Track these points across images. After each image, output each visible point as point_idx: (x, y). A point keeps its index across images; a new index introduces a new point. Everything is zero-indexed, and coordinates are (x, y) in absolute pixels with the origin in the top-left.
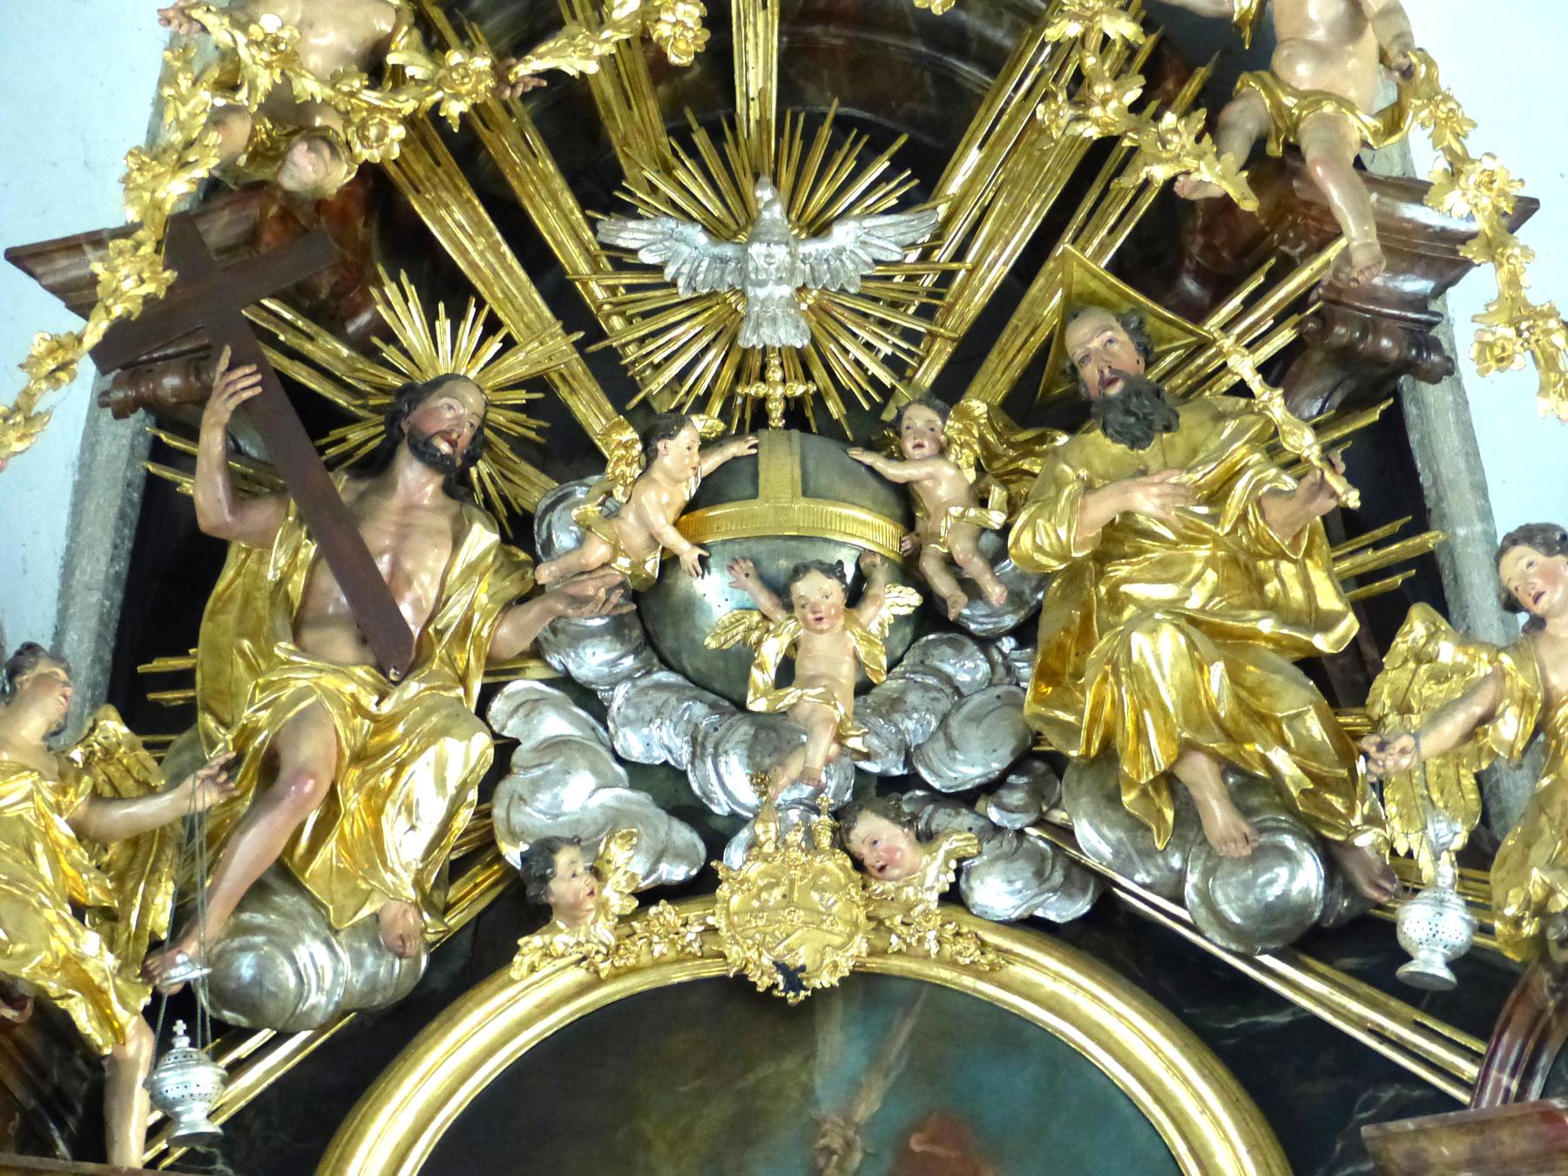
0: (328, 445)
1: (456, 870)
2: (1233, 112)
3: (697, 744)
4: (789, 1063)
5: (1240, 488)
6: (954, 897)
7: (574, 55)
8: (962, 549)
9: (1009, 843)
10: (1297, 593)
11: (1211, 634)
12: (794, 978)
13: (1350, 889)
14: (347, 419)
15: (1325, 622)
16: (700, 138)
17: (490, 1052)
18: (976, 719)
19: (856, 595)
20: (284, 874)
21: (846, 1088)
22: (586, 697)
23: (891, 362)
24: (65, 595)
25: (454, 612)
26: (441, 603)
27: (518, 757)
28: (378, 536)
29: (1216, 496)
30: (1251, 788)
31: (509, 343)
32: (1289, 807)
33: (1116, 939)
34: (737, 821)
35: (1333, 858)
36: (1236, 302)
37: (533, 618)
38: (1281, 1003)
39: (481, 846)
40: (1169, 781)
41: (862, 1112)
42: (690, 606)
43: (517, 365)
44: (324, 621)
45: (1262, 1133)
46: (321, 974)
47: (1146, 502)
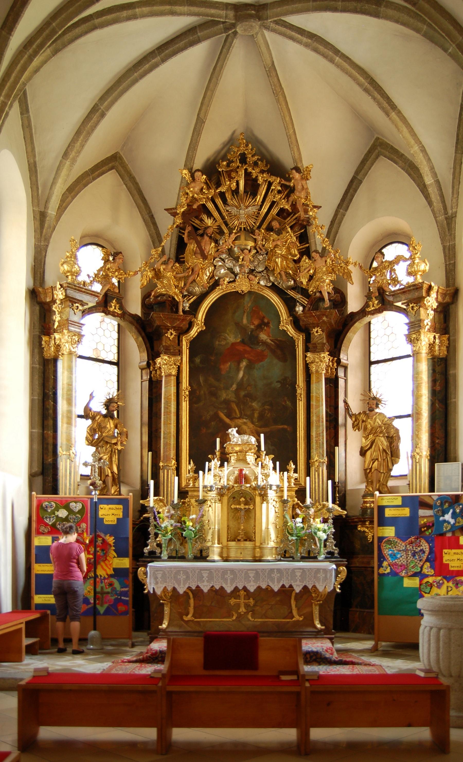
0: (198, 233)
1: (211, 279)
2: (290, 198)
3: (234, 266)
4: (242, 300)
5: (288, 241)
6: (259, 283)
7: (222, 189)
8: (261, 246)
9: (264, 277)
10: (294, 252)
11: (284, 257)
12: (243, 291)
13: (296, 284)
14: (200, 230)
15: (296, 256)
16: (235, 196)
17: (214, 298)
18: (261, 264)
19: (250, 251)
20: (194, 281)
21: (247, 303)
22: (223, 260)
23: (254, 223)
24: (171, 244)
25: (210, 253)
26: (209, 251)
27: (216, 267)
28: (203, 244)
29: (286, 242)
30: (287, 274)
31: (216, 221)
32: (291, 276)
33: (274, 288)
34: (238, 274)
35: (295, 281)
36: (289, 218)
37: (218, 253)
38: (289, 295)
39: (213, 276)
40: (279, 273)
41: (249, 306)
42: (234, 251)
43: (217, 224)
44: (198, 253)
45: (286, 308)
46: (197, 290)
47: (279, 243)
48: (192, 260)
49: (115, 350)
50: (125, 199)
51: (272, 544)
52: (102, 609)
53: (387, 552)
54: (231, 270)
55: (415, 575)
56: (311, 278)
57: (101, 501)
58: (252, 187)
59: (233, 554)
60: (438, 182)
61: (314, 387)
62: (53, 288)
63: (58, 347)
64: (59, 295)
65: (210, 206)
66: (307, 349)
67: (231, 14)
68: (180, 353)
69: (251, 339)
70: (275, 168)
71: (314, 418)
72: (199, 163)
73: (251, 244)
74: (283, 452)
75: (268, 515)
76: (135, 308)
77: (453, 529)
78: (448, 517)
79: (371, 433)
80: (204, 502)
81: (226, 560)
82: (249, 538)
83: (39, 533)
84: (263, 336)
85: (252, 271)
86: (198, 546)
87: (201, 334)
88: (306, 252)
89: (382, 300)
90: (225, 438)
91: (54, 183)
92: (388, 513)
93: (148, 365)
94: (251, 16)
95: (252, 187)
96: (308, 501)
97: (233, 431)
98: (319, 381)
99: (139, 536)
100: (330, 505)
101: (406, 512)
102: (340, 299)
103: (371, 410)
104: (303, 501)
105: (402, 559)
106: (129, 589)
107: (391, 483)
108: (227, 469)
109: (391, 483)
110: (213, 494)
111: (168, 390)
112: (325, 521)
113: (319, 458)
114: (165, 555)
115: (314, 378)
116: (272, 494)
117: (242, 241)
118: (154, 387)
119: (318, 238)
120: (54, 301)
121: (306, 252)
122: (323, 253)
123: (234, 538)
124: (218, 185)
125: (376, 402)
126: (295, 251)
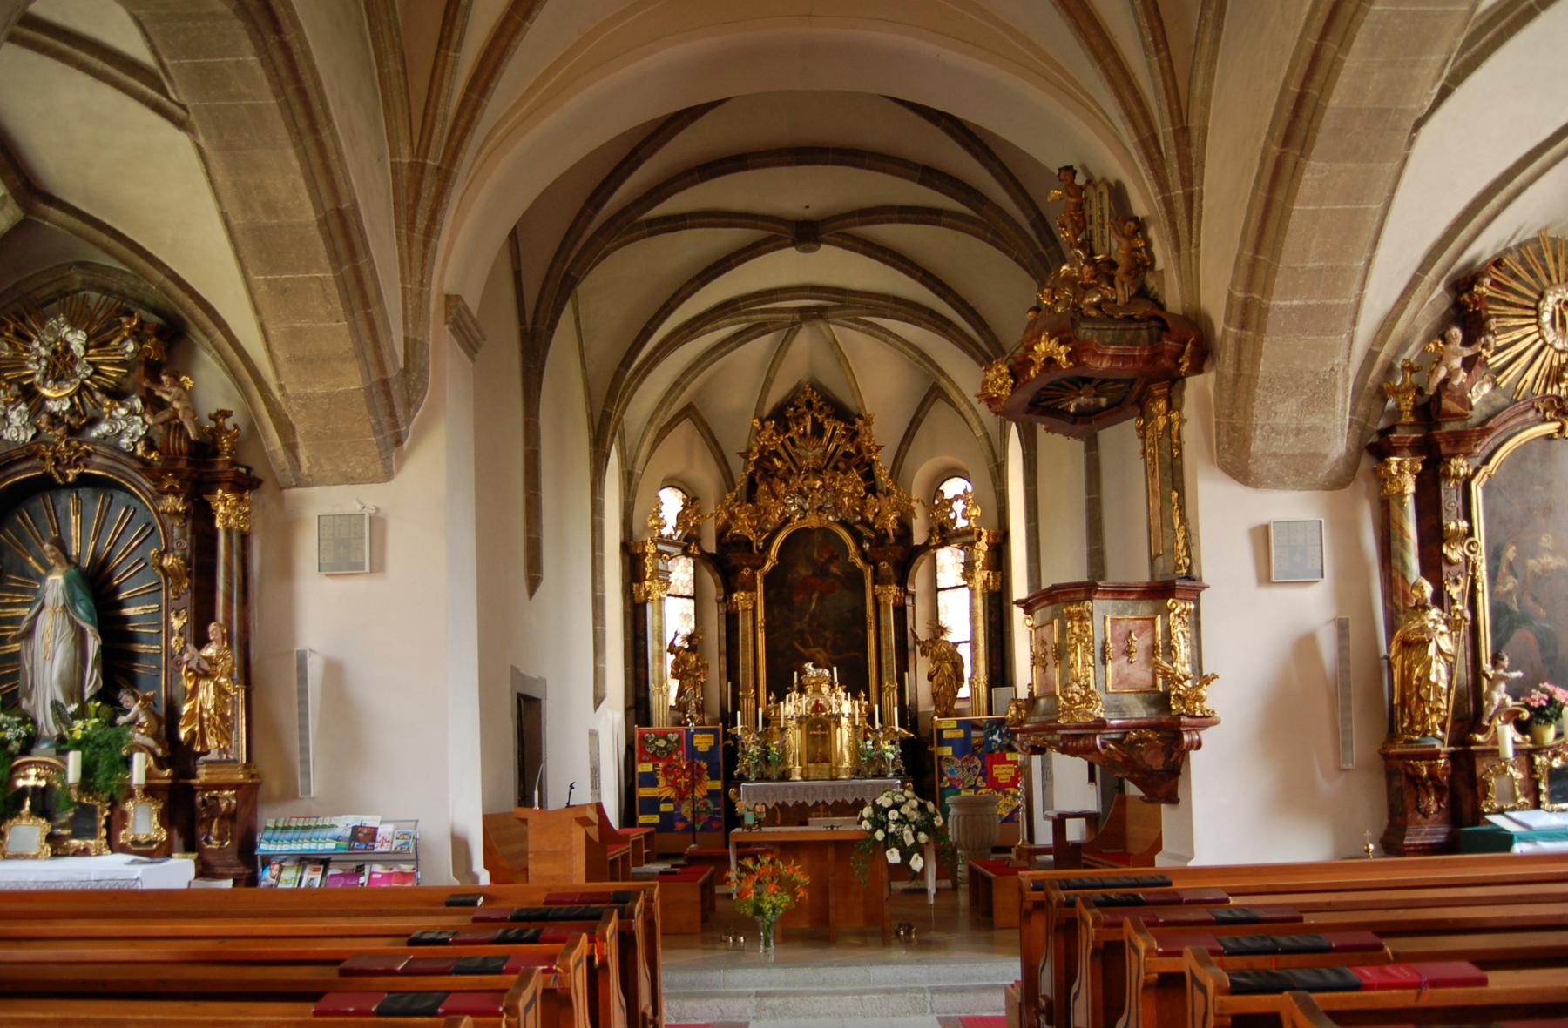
11: (851, 495)
21: (818, 537)
33: (843, 523)
48: (764, 500)
49: (691, 585)
50: (698, 438)
51: (846, 765)
52: (698, 827)
53: (946, 768)
54: (801, 507)
55: (970, 787)
56: (877, 515)
57: (697, 731)
58: (818, 430)
59: (812, 775)
60: (987, 434)
61: (882, 617)
62: (644, 543)
63: (648, 593)
64: (651, 549)
65: (782, 451)
66: (875, 582)
67: (797, 316)
68: (754, 589)
69: (822, 572)
70: (842, 412)
71: (884, 646)
72: (767, 410)
73: (818, 483)
74: (855, 683)
75: (843, 737)
76: (711, 546)
77: (1001, 747)
78: (995, 737)
79: (937, 659)
80: (785, 729)
81: (806, 779)
82: (826, 759)
83: (642, 761)
84: (833, 569)
85: (820, 509)
86: (782, 768)
87: (774, 568)
89: (944, 534)
90: (802, 672)
91: (640, 446)
92: (946, 735)
93: (725, 600)
94: (814, 318)
95: (818, 430)
96: (878, 725)
97: (809, 666)
98: (887, 611)
99: (727, 759)
100: (897, 729)
101: (961, 733)
102: (905, 529)
104: (873, 724)
105: (958, 775)
107: (957, 705)
108: (805, 699)
109: (957, 705)
110: (794, 722)
111: (744, 624)
112: (892, 743)
113: (890, 685)
114: (752, 777)
115: (882, 609)
116: (844, 721)
117: (810, 482)
118: (731, 620)
119: (883, 477)
120: (645, 554)
121: (872, 489)
122: (888, 493)
123: (812, 760)
124: (787, 430)
125: (943, 630)
126: (860, 489)
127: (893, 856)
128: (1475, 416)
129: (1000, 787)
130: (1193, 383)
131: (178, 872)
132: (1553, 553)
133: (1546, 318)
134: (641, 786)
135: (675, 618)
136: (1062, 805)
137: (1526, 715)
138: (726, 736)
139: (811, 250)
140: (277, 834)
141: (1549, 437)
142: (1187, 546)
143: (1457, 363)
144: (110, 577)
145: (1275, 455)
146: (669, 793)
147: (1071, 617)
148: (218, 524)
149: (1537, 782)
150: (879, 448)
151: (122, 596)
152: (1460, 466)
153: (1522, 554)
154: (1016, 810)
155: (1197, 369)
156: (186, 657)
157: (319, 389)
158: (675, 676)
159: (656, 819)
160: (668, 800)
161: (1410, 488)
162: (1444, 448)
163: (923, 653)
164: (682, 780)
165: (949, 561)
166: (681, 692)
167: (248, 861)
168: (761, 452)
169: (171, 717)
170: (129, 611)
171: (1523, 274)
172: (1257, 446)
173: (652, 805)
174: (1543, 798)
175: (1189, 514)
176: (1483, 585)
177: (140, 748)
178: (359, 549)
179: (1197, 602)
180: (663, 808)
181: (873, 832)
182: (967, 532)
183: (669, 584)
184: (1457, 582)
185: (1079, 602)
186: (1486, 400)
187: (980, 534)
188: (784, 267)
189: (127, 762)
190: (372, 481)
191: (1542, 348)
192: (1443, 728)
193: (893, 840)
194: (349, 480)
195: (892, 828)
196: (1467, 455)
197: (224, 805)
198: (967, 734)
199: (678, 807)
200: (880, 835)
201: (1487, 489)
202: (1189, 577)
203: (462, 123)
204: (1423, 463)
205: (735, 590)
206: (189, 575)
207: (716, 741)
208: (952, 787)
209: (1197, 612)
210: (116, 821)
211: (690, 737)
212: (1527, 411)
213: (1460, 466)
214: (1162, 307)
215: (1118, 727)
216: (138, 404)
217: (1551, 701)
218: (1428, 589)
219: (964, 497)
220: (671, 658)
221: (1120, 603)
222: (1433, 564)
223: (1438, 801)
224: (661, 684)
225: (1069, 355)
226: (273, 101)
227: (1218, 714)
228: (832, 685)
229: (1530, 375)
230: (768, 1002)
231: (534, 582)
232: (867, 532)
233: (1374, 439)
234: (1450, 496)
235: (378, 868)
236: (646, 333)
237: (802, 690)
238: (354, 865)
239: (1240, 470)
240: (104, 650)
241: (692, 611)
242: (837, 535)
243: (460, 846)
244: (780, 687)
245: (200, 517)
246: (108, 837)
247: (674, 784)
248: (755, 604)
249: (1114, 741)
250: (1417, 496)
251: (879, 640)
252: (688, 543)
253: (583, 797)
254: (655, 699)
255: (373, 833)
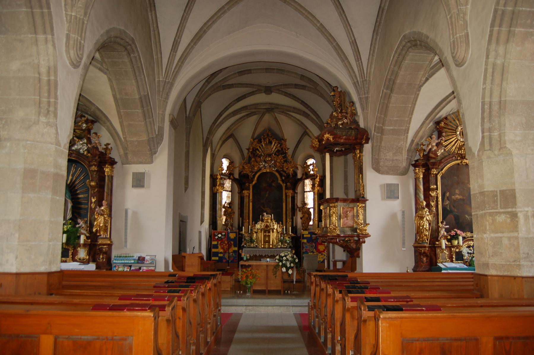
11: (279, 163)
33: (277, 171)
54: (264, 165)
57: (230, 232)
61: (288, 200)
62: (217, 175)
63: (217, 190)
64: (219, 177)
72: (255, 136)
74: (278, 219)
75: (273, 236)
76: (237, 176)
83: (214, 241)
84: (273, 184)
87: (255, 184)
88: (286, 161)
89: (307, 175)
90: (263, 216)
92: (305, 236)
99: (239, 240)
101: (309, 236)
102: (295, 174)
103: (303, 206)
106: (237, 256)
107: (309, 227)
111: (246, 200)
116: (275, 230)
118: (242, 199)
120: (217, 178)
122: (291, 162)
127: (284, 270)
128: (439, 158)
129: (320, 252)
130: (366, 146)
131: (92, 267)
132: (459, 195)
133: (458, 133)
134: (213, 248)
135: (225, 197)
136: (337, 258)
137: (449, 237)
138: (239, 234)
139: (269, 94)
140: (118, 258)
141: (458, 164)
142: (363, 189)
143: (434, 144)
144: (75, 187)
145: (386, 166)
146: (222, 251)
147: (332, 207)
148: (106, 174)
149: (452, 255)
150: (288, 149)
151: (78, 192)
152: (434, 171)
153: (451, 195)
154: (324, 260)
155: (367, 142)
156: (97, 210)
157: (135, 139)
158: (224, 215)
159: (217, 258)
160: (221, 253)
161: (422, 176)
162: (430, 166)
163: (299, 211)
164: (226, 247)
165: (308, 183)
166: (226, 220)
167: (109, 264)
168: (253, 149)
169: (91, 226)
170: (80, 196)
171: (453, 121)
172: (382, 164)
173: (216, 254)
174: (454, 259)
175: (364, 181)
176: (440, 203)
177: (83, 234)
178: (139, 181)
179: (365, 203)
180: (220, 255)
181: (278, 263)
182: (313, 175)
183: (224, 187)
184: (433, 201)
185: (334, 203)
186: (442, 154)
187: (317, 176)
188: (261, 98)
189: (79, 237)
190: (147, 163)
191: (457, 141)
192: (427, 240)
193: (284, 265)
194: (141, 163)
195: (284, 262)
196: (436, 169)
197: (104, 250)
198: (311, 236)
199: (224, 255)
200: (280, 264)
201: (442, 178)
202: (363, 197)
203: (176, 70)
204: (425, 170)
205: (243, 190)
206: (97, 187)
207: (236, 235)
208: (306, 252)
209: (365, 206)
210: (75, 254)
211: (228, 233)
212: (453, 157)
213: (434, 171)
214: (359, 125)
215: (343, 237)
216: (85, 141)
217: (456, 234)
218: (425, 203)
219: (313, 164)
220: (223, 210)
221: (345, 204)
222: (427, 197)
223: (427, 259)
224: (220, 217)
225: (333, 138)
226: (131, 70)
227: (370, 234)
228: (271, 220)
229: (454, 148)
230: (248, 308)
231: (186, 190)
232: (284, 174)
233: (414, 163)
234: (432, 179)
235: (145, 268)
236: (220, 115)
237: (262, 221)
238: (138, 267)
239: (377, 169)
240: (73, 207)
241: (230, 196)
242: (275, 174)
243: (166, 262)
244: (256, 220)
245: (101, 172)
246: (72, 257)
247: (223, 248)
248: (249, 194)
249: (342, 240)
250: (423, 178)
251: (286, 206)
252: (230, 175)
253: (196, 251)
254: (219, 222)
255: (144, 258)
